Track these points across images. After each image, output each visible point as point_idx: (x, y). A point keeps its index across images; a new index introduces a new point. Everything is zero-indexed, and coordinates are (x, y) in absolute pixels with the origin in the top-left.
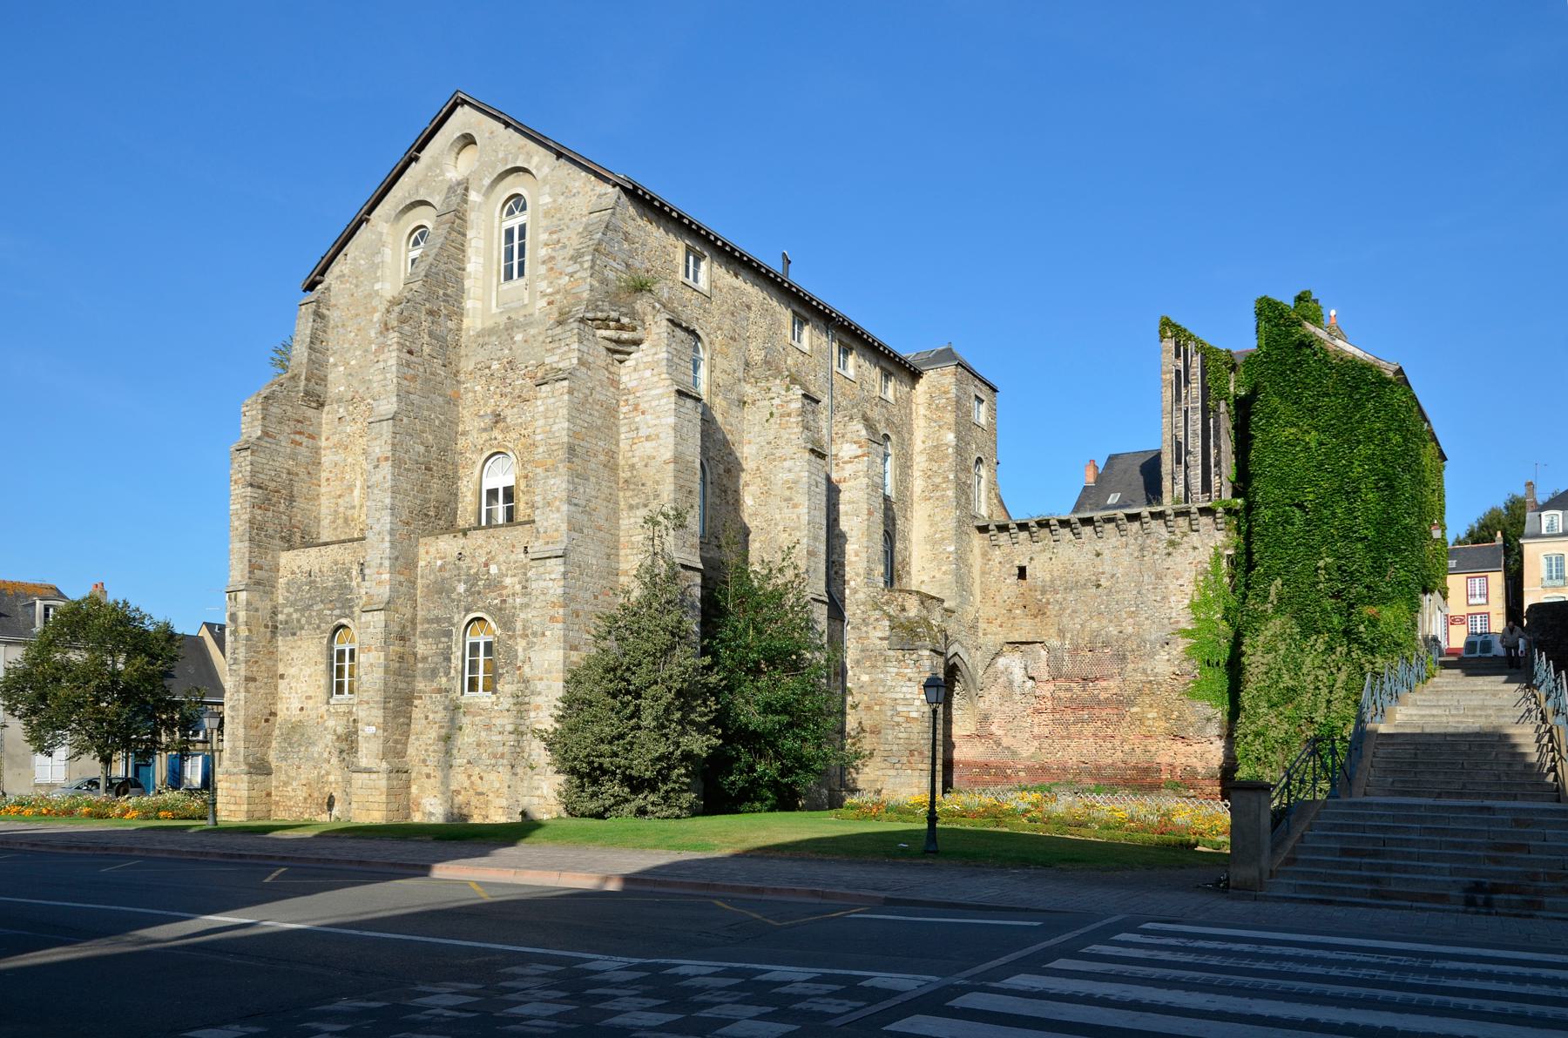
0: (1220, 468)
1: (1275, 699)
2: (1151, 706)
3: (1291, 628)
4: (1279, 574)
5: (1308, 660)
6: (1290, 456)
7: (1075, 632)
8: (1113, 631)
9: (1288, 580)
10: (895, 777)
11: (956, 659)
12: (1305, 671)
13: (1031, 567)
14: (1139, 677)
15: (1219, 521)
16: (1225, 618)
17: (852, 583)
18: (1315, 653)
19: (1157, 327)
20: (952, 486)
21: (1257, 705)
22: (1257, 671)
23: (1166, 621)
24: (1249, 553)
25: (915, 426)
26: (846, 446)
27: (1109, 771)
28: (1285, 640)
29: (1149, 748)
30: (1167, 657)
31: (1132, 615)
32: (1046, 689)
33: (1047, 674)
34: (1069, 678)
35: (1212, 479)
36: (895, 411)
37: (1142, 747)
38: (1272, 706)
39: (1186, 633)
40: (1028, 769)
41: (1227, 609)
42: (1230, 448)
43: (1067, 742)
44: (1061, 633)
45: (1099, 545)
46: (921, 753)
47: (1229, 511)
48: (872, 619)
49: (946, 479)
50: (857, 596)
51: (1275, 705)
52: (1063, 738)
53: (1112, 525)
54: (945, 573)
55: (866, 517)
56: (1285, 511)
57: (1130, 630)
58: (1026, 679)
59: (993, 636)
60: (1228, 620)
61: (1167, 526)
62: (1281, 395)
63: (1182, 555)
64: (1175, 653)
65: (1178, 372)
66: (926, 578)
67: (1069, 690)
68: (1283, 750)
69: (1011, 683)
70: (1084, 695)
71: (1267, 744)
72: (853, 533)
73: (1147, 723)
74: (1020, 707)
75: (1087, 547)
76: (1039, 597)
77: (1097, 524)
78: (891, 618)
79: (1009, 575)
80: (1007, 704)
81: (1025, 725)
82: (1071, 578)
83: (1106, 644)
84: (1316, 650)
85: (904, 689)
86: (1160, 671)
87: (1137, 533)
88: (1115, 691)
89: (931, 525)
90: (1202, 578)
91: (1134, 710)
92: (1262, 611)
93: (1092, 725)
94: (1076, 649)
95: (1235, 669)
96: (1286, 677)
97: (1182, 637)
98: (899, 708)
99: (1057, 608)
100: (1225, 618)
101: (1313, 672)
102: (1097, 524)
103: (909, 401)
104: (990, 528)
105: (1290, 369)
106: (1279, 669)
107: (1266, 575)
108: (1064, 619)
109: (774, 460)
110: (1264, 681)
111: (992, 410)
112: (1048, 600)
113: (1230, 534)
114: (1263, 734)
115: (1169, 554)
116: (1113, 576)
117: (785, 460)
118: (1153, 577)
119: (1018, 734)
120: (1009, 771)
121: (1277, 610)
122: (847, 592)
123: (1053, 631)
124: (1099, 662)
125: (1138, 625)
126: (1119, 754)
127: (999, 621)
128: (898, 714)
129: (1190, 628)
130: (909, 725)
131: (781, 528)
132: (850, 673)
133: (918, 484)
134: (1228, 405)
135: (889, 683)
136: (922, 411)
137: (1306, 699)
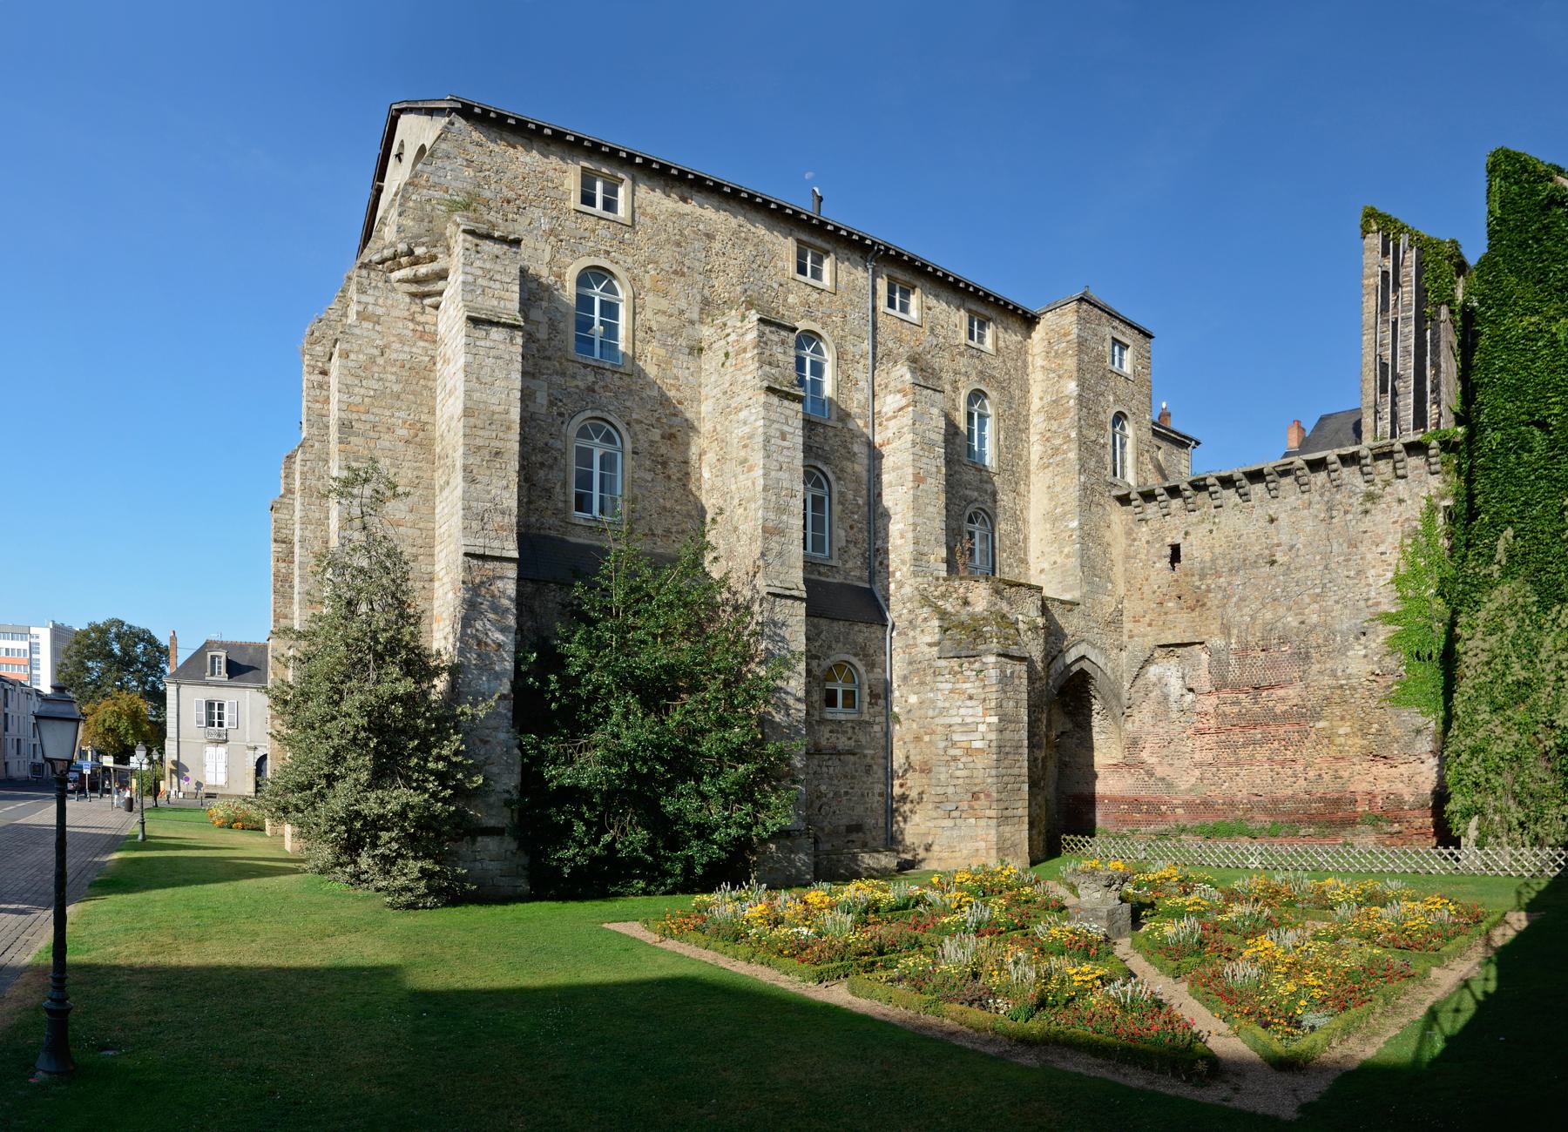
0: (1439, 394)
1: (1501, 699)
2: (1342, 718)
3: (1524, 596)
4: (1510, 522)
5: (1548, 641)
6: (1530, 355)
7: (1244, 627)
8: (1292, 621)
9: (1523, 529)
10: (952, 828)
11: (1085, 665)
12: (1543, 656)
13: (1187, 544)
14: (1327, 681)
15: (1433, 460)
16: (1440, 594)
17: (898, 574)
18: (1558, 630)
19: (1358, 220)
20: (1074, 446)
21: (1475, 711)
22: (1475, 660)
23: (1362, 603)
24: (1471, 497)
25: (1031, 382)
26: (890, 399)
27: (1290, 805)
28: (1515, 614)
29: (1341, 773)
30: (1363, 652)
31: (1317, 598)
32: (1209, 703)
33: (1208, 684)
34: (1236, 688)
35: (1428, 408)
36: (997, 362)
37: (1331, 772)
38: (1497, 709)
39: (1389, 618)
40: (1187, 805)
41: (1442, 580)
42: (1455, 369)
43: (1235, 770)
44: (1226, 630)
45: (1273, 508)
46: (988, 796)
47: (1447, 446)
48: (920, 619)
49: (1067, 439)
50: (903, 591)
51: (1501, 708)
52: (1230, 764)
53: (1289, 480)
54: (1067, 556)
55: (911, 485)
56: (1520, 433)
57: (1315, 618)
58: (1185, 692)
59: (1143, 637)
60: (1443, 596)
61: (1362, 473)
62: (1518, 272)
63: (1384, 511)
64: (1373, 645)
65: (1385, 274)
66: (1046, 566)
67: (1236, 703)
68: (1512, 768)
69: (1166, 697)
70: (1256, 708)
71: (1488, 764)
72: (899, 509)
73: (1339, 740)
74: (1177, 728)
75: (1258, 512)
76: (1198, 583)
77: (1268, 478)
78: (943, 615)
79: (1160, 557)
80: (1161, 724)
81: (1185, 749)
82: (1237, 555)
83: (1283, 640)
84: (1559, 626)
85: (962, 711)
86: (1354, 671)
87: (1323, 486)
88: (1295, 702)
89: (1051, 499)
90: (1410, 541)
91: (1321, 724)
92: (1485, 576)
93: (1266, 747)
94: (1245, 649)
95: (1449, 660)
96: (1516, 667)
97: (1384, 624)
98: (956, 737)
99: (1219, 596)
100: (1440, 594)
101: (1555, 657)
102: (1268, 478)
103: (1022, 352)
104: (1132, 497)
105: (1531, 238)
106: (1506, 656)
107: (1493, 524)
108: (1229, 610)
109: (730, 413)
110: (1485, 675)
111: (1143, 358)
112: (1208, 586)
113: (1449, 478)
114: (1483, 750)
115: (1366, 512)
116: (1292, 547)
117: (741, 410)
118: (1345, 545)
119: (1176, 762)
120: (1164, 808)
121: (1507, 573)
122: (892, 587)
123: (1215, 627)
124: (1274, 665)
125: (1325, 611)
126: (1302, 782)
127: (1147, 619)
128: (954, 744)
129: (1394, 611)
130: (970, 759)
131: (736, 502)
132: (896, 694)
133: (1035, 450)
134: (1452, 312)
135: (940, 704)
136: (1039, 362)
137: (1543, 696)
